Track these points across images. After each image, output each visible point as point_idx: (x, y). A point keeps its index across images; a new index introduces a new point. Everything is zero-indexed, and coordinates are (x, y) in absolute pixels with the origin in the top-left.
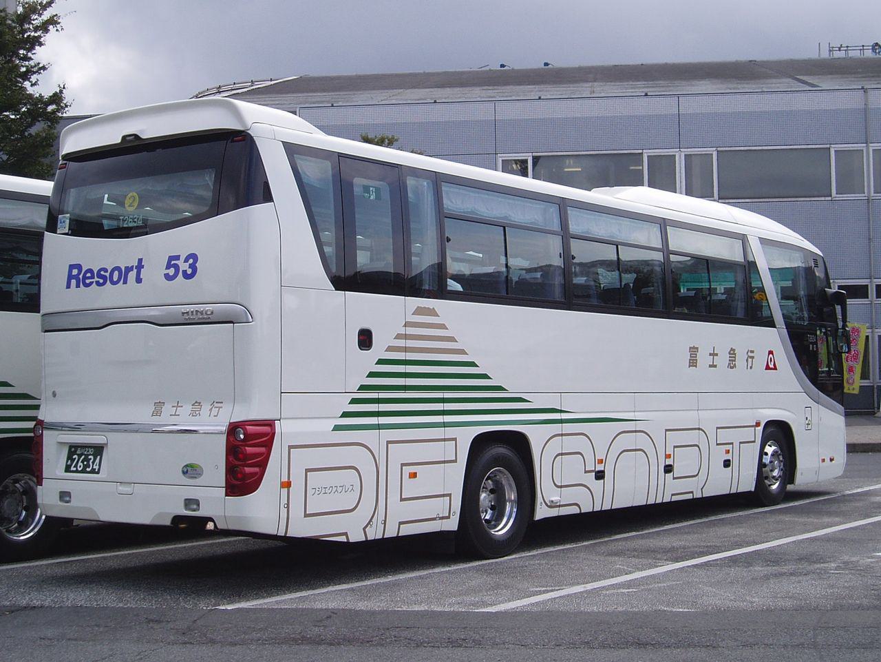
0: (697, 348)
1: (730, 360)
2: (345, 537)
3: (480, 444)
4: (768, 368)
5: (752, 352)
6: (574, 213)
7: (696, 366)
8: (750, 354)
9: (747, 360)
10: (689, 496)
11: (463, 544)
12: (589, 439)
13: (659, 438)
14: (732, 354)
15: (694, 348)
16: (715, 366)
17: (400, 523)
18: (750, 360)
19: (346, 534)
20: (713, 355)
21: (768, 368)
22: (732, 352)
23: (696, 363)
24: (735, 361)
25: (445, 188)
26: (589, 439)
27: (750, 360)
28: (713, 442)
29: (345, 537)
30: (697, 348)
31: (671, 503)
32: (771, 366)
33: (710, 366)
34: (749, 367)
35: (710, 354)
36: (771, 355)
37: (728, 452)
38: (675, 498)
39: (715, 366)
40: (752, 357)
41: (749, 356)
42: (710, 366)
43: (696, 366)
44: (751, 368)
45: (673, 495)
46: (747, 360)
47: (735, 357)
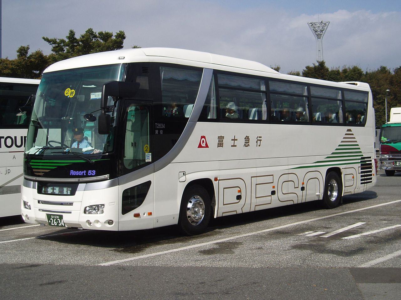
0: (223, 137)
1: (245, 142)
2: (236, 212)
3: (329, 171)
4: (200, 146)
5: (261, 137)
6: (220, 76)
7: (222, 147)
8: (259, 139)
9: (257, 142)
10: (235, 213)
11: (180, 231)
12: (296, 175)
13: (248, 182)
14: (247, 139)
15: (221, 137)
16: (236, 146)
17: (256, 206)
18: (259, 142)
19: (236, 211)
20: (234, 140)
21: (200, 146)
22: (247, 138)
23: (223, 145)
24: (249, 142)
25: (219, 75)
26: (296, 175)
27: (259, 142)
28: (357, 173)
29: (236, 212)
30: (223, 137)
31: (222, 217)
32: (204, 145)
33: (232, 146)
34: (258, 146)
35: (232, 140)
36: (203, 139)
37: (274, 187)
38: (224, 215)
39: (236, 146)
40: (260, 140)
41: (258, 140)
42: (232, 146)
43: (222, 147)
44: (259, 146)
45: (223, 213)
46: (257, 142)
47: (249, 141)
